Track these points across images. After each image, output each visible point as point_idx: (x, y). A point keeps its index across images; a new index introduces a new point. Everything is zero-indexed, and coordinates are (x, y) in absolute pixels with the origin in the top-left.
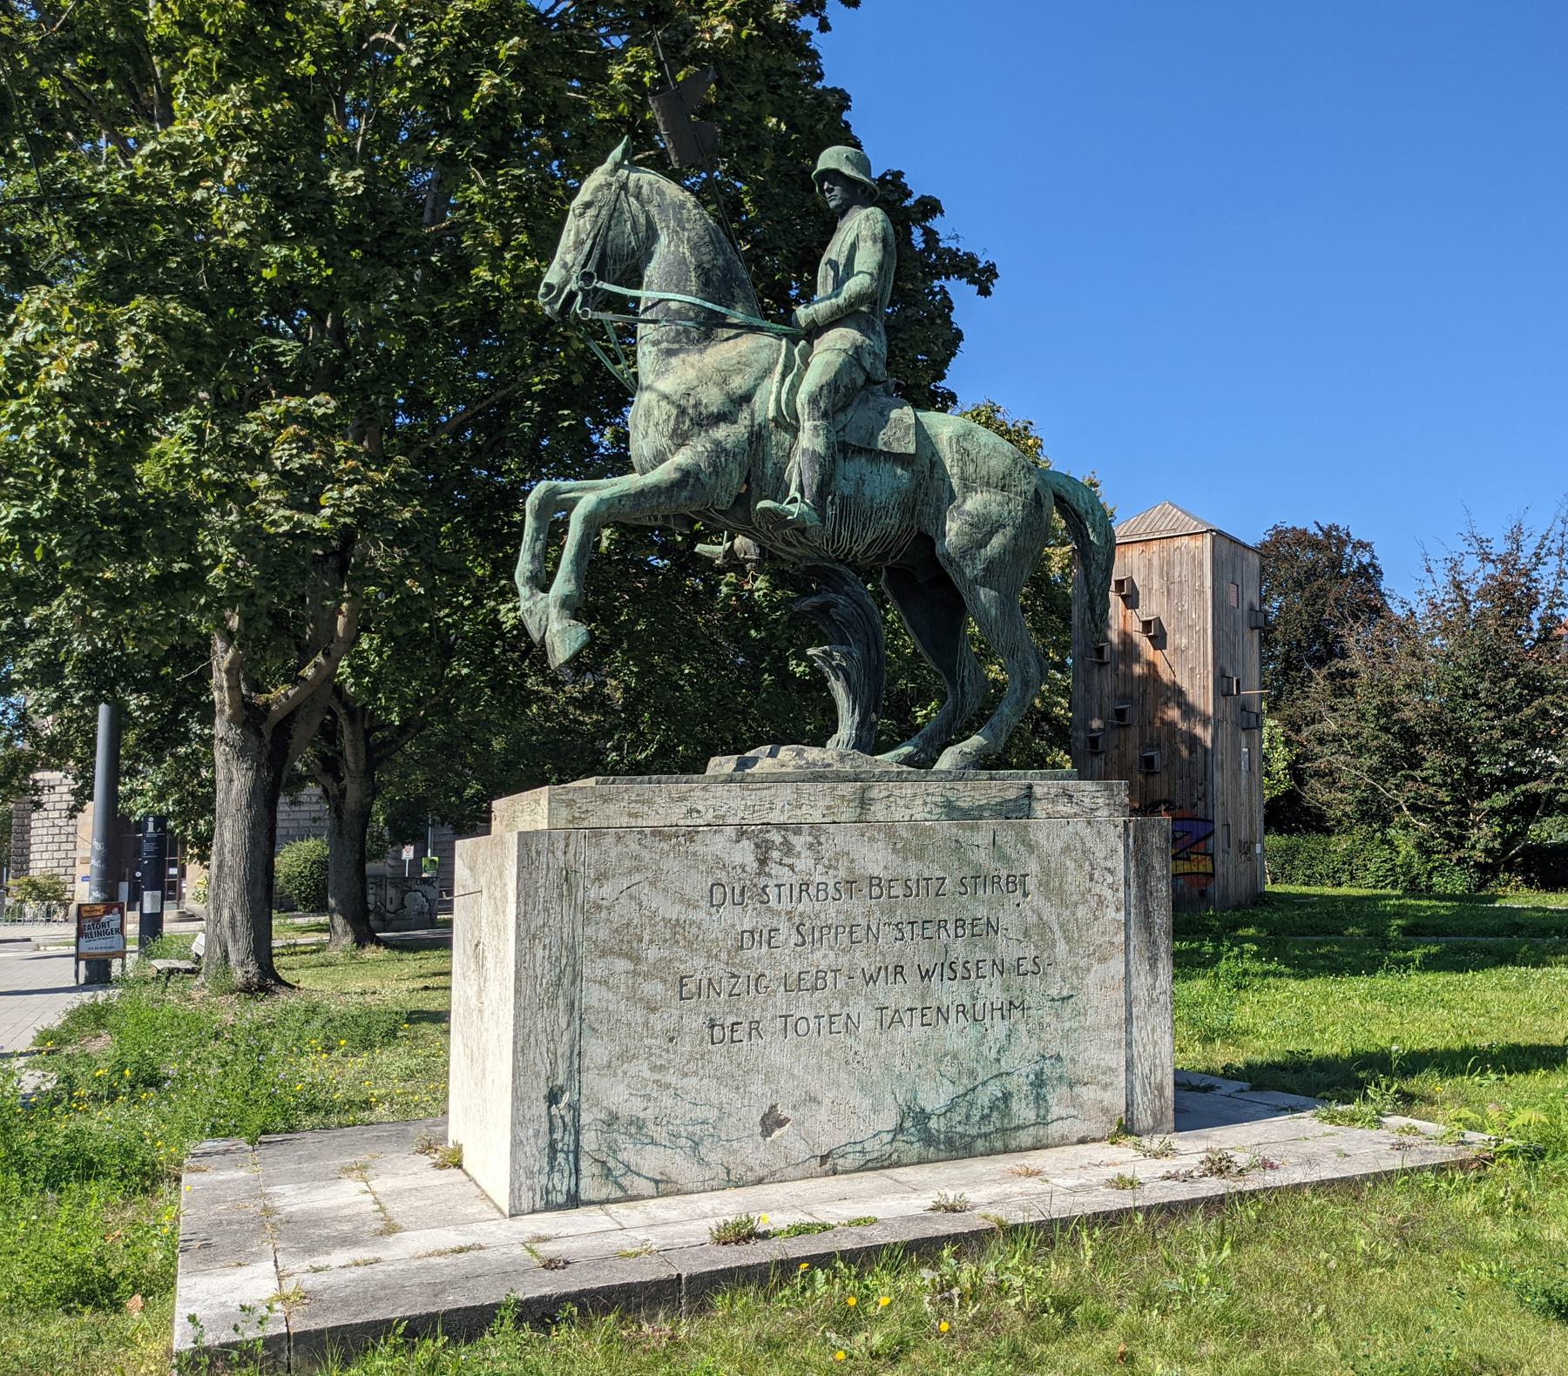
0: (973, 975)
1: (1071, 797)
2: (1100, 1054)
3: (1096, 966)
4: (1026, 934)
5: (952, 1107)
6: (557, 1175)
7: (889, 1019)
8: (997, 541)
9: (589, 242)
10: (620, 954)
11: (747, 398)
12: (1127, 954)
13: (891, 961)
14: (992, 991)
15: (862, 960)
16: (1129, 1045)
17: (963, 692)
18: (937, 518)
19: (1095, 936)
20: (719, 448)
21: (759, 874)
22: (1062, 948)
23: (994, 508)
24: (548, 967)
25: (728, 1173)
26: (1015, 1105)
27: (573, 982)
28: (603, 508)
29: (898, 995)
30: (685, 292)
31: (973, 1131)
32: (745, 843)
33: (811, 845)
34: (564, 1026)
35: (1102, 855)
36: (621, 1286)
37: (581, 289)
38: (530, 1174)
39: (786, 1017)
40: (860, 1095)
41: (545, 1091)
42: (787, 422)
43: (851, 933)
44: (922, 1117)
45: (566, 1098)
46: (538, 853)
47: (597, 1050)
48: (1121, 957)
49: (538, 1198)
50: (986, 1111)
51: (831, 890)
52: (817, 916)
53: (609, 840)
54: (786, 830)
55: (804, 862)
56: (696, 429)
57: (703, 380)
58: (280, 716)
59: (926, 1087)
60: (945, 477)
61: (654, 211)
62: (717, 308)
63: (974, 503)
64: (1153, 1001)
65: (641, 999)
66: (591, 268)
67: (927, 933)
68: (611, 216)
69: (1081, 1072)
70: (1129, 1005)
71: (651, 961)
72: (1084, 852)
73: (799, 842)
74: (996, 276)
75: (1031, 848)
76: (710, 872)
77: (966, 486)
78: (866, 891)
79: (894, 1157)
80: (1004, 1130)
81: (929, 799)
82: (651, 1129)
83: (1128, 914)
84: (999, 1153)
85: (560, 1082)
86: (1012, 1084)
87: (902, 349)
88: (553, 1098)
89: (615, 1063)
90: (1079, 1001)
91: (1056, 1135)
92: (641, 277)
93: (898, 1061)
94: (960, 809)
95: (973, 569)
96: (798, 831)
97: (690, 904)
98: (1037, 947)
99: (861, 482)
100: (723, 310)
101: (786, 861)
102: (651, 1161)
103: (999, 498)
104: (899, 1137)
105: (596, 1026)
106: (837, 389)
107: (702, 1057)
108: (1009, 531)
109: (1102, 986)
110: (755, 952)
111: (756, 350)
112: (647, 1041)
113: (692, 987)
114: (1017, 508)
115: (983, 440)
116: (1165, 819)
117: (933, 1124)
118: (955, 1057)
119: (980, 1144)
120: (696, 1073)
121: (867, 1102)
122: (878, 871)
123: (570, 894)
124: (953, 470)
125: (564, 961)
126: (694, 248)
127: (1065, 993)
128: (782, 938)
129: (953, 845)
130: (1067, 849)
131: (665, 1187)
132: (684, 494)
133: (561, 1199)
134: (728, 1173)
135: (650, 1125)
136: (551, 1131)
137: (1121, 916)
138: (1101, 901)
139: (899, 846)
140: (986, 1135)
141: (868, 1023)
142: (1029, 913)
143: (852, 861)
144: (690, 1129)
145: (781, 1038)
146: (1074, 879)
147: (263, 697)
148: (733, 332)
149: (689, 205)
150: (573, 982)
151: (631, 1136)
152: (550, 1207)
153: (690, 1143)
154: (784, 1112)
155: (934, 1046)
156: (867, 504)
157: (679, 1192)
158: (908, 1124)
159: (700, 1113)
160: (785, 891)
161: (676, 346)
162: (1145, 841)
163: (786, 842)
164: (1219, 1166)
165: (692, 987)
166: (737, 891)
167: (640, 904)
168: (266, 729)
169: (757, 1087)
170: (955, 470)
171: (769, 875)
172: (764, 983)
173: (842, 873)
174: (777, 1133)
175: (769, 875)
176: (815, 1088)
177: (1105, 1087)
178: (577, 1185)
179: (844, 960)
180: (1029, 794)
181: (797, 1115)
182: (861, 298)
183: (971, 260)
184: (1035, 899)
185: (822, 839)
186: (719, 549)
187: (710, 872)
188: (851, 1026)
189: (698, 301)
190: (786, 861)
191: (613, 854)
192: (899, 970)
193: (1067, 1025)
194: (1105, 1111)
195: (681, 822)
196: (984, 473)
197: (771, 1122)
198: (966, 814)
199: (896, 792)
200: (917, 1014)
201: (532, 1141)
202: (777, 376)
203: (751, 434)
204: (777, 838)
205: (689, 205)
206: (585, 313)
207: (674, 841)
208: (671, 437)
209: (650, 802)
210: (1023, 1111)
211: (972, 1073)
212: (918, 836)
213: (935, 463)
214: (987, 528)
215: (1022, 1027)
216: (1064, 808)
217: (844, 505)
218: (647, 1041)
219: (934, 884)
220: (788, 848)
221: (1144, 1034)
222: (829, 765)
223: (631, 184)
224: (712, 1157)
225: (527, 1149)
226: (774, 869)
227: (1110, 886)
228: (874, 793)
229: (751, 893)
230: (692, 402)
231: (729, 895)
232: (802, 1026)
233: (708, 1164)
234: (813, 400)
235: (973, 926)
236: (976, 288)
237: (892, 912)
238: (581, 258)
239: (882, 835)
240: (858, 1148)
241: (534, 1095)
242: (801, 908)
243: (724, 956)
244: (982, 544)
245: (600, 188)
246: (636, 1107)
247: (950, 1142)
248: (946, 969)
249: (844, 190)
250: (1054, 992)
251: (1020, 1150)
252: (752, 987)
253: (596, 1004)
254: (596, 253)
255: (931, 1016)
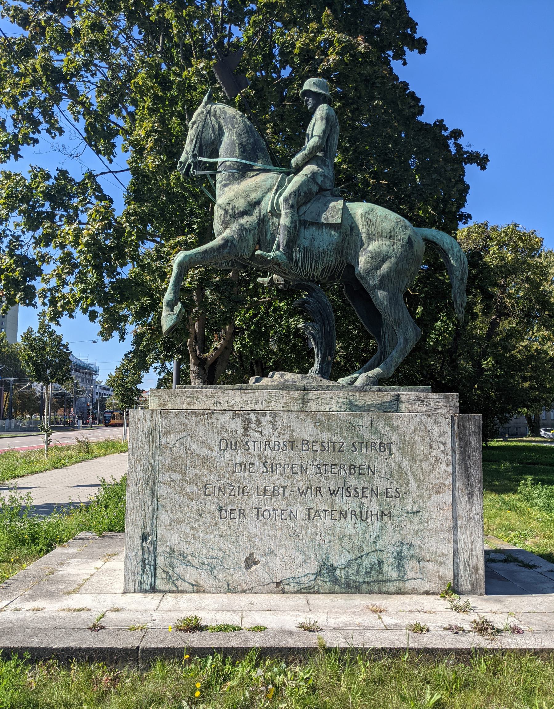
0: (360, 495)
1: (423, 401)
2: (438, 545)
3: (434, 496)
4: (391, 475)
5: (349, 565)
6: (145, 576)
7: (313, 515)
8: (386, 266)
9: (195, 140)
10: (176, 471)
11: (258, 203)
12: (453, 490)
13: (314, 484)
14: (372, 505)
15: (298, 483)
16: (455, 542)
17: (385, 347)
18: (355, 256)
19: (433, 479)
20: (243, 228)
21: (244, 435)
22: (413, 484)
23: (385, 248)
24: (142, 475)
25: (228, 585)
26: (385, 568)
27: (154, 483)
28: (187, 259)
29: (320, 502)
30: (233, 157)
31: (361, 580)
32: (237, 419)
33: (271, 422)
34: (150, 504)
35: (437, 434)
36: (108, 648)
37: (192, 162)
38: (133, 574)
39: (258, 508)
40: (297, 553)
41: (141, 535)
42: (275, 213)
43: (292, 468)
44: (332, 569)
45: (150, 539)
46: (139, 420)
47: (165, 517)
48: (450, 492)
49: (137, 586)
50: (368, 570)
51: (281, 446)
52: (274, 458)
53: (171, 415)
54: (258, 414)
55: (267, 430)
56: (233, 219)
57: (237, 196)
58: (211, 363)
59: (334, 552)
60: (359, 234)
61: (222, 121)
62: (248, 162)
63: (373, 246)
64: (470, 519)
65: (186, 494)
66: (196, 152)
67: (334, 471)
68: (203, 127)
69: (424, 554)
70: (455, 519)
71: (191, 475)
72: (426, 432)
73: (264, 420)
74: (489, 161)
75: (394, 429)
76: (219, 433)
77: (369, 238)
78: (300, 446)
79: (316, 588)
80: (379, 581)
81: (339, 400)
82: (190, 558)
83: (454, 468)
84: (376, 593)
85: (147, 530)
86: (383, 556)
87: (430, 194)
88: (144, 538)
89: (173, 524)
90: (424, 514)
91: (410, 588)
92: (218, 152)
93: (318, 537)
94: (357, 406)
95: (373, 281)
96: (264, 415)
97: (210, 448)
98: (397, 483)
99: (313, 239)
100: (251, 163)
101: (258, 429)
102: (191, 574)
103: (388, 243)
104: (319, 578)
105: (165, 505)
106: (300, 194)
107: (216, 525)
108: (393, 260)
109: (438, 507)
110: (242, 474)
111: (264, 181)
112: (189, 515)
113: (210, 489)
114: (398, 247)
115: (379, 214)
116: (478, 417)
117: (338, 573)
118: (350, 538)
119: (365, 587)
120: (213, 533)
121: (301, 557)
122: (306, 437)
123: (153, 440)
124: (362, 229)
125: (150, 472)
126: (239, 136)
127: (415, 509)
128: (256, 468)
129: (348, 425)
130: (415, 430)
131: (197, 589)
132: (226, 251)
133: (147, 587)
134: (228, 585)
135: (190, 557)
136: (143, 554)
137: (450, 469)
138: (437, 460)
139: (318, 424)
140: (368, 583)
141: (301, 516)
142: (393, 464)
143: (293, 431)
144: (209, 560)
145: (256, 519)
146: (420, 447)
147: (205, 355)
148: (255, 173)
149: (237, 116)
150: (154, 483)
151: (180, 561)
152: (142, 591)
153: (209, 568)
154: (257, 558)
155: (338, 531)
156: (316, 251)
157: (204, 592)
158: (324, 571)
159: (214, 553)
160: (257, 444)
161: (228, 182)
162: (465, 427)
163: (258, 420)
164: (483, 628)
165: (210, 489)
166: (233, 443)
167: (186, 447)
168: (206, 367)
169: (243, 543)
170: (364, 230)
171: (249, 436)
172: (247, 490)
173: (287, 437)
174: (254, 568)
175: (249, 436)
176: (273, 547)
177: (441, 564)
178: (155, 582)
179: (288, 482)
180: (397, 399)
181: (264, 560)
182: (315, 149)
183: (478, 154)
184: (397, 456)
185: (277, 419)
186: (266, 280)
187: (219, 433)
188: (292, 516)
189: (239, 160)
190: (258, 429)
191: (173, 422)
192: (318, 489)
193: (417, 527)
194: (440, 578)
195: (212, 408)
196: (379, 230)
197: (250, 562)
198: (361, 409)
199: (322, 396)
200: (328, 513)
201: (134, 558)
202: (273, 191)
203: (259, 220)
204: (253, 417)
205: (237, 116)
206: (194, 173)
207: (202, 417)
208: (222, 225)
209: (197, 398)
210: (390, 572)
211: (360, 548)
212: (328, 420)
213: (353, 227)
214: (381, 259)
215: (389, 526)
216: (418, 407)
217: (306, 252)
218: (189, 515)
219: (337, 446)
220: (259, 423)
221: (465, 536)
222: (295, 382)
223: (212, 111)
224: (220, 576)
225: (132, 561)
226: (252, 433)
227: (443, 452)
228: (310, 396)
229: (238, 444)
230: (231, 206)
231: (229, 445)
232: (266, 514)
233: (218, 580)
234: (286, 200)
235: (360, 469)
236: (479, 167)
237: (314, 458)
238: (192, 147)
239: (308, 418)
240: (296, 581)
241: (135, 536)
242: (265, 453)
243: (226, 475)
244: (378, 267)
245: (199, 114)
246: (182, 546)
247: (347, 584)
248: (344, 491)
249: (313, 99)
250: (408, 508)
251: (388, 593)
252: (241, 492)
253: (165, 494)
254: (198, 144)
255: (336, 515)
